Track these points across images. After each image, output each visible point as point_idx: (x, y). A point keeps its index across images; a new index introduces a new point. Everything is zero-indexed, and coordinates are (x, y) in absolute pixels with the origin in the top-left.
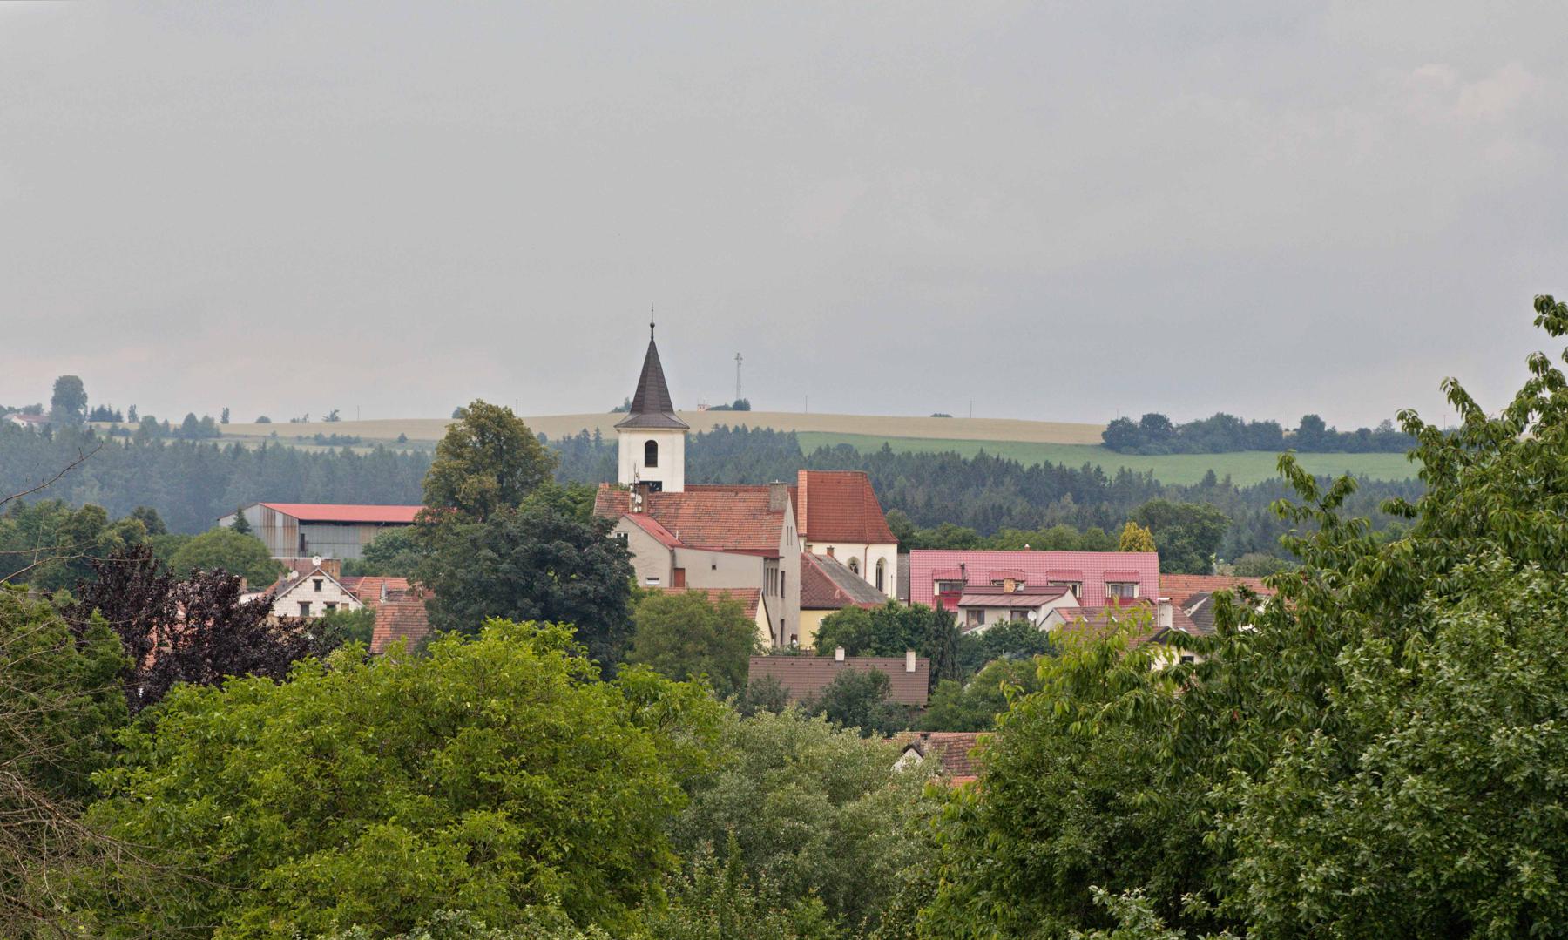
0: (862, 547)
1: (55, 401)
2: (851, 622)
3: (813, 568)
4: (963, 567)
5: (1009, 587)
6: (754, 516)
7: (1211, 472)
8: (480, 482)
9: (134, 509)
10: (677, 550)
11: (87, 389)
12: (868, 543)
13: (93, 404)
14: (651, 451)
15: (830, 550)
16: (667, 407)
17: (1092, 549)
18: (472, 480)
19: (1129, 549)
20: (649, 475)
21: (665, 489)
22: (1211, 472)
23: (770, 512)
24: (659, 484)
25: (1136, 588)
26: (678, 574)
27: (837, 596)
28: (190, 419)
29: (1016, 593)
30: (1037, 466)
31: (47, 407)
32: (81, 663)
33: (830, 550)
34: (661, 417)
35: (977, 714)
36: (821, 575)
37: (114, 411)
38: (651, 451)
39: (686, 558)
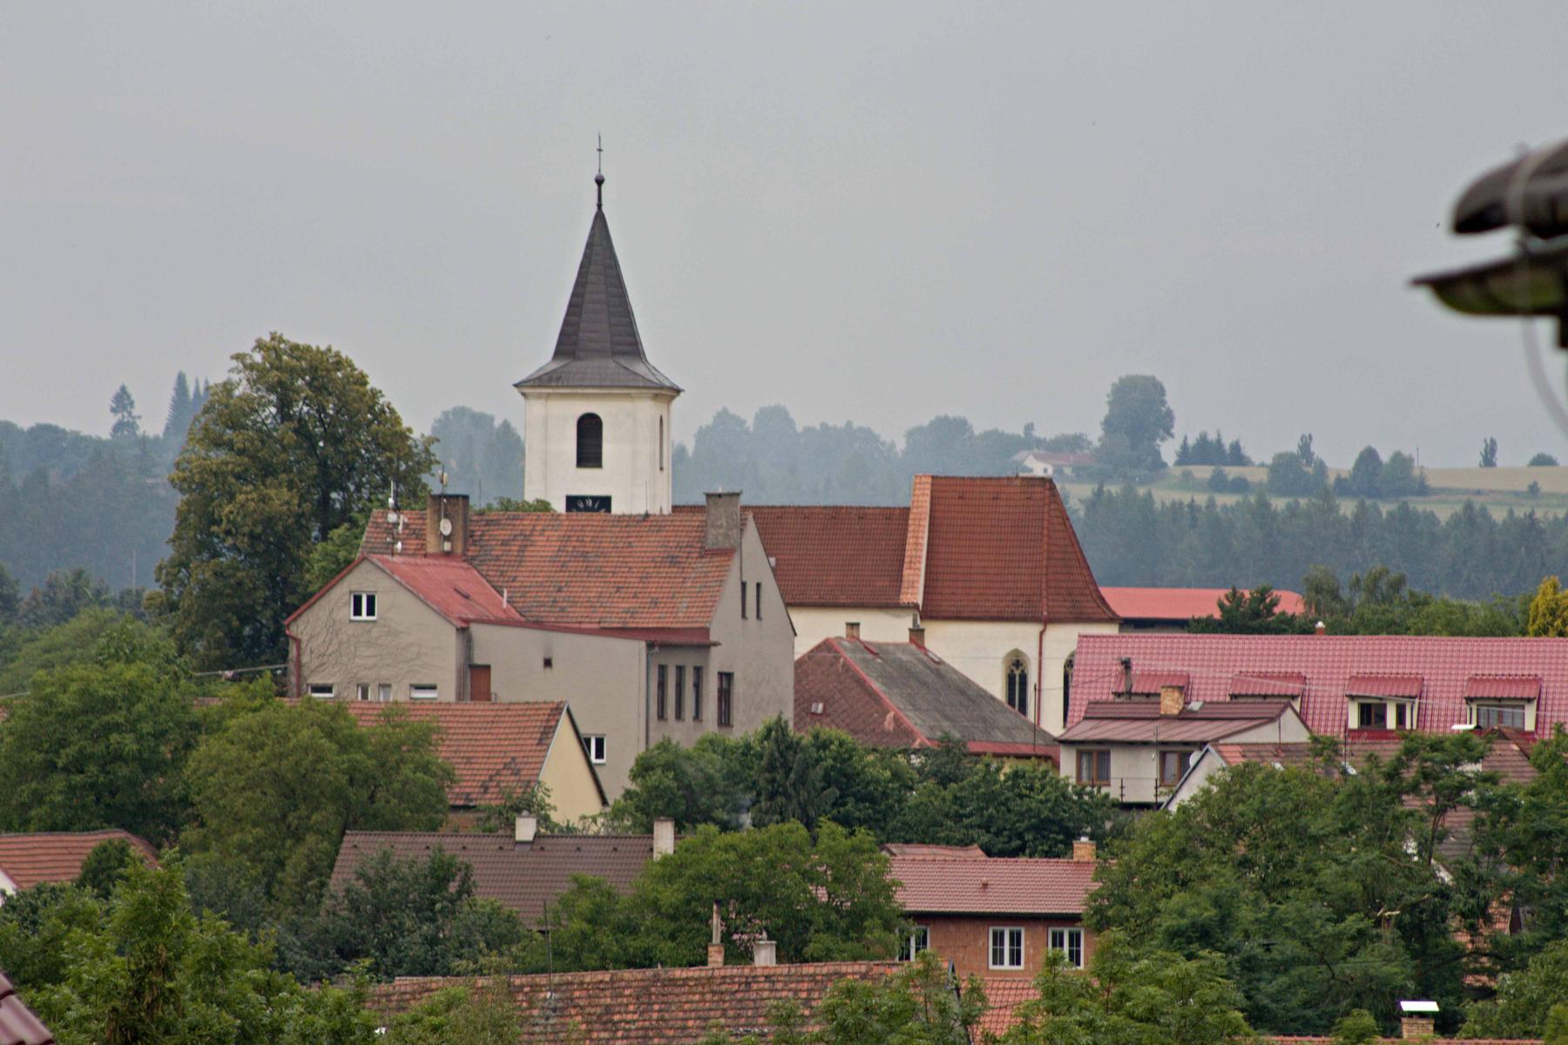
0: (1033, 629)
1: (1109, 424)
2: (667, 767)
3: (847, 667)
4: (1127, 664)
5: (1170, 703)
6: (673, 561)
7: (123, 389)
8: (264, 499)
9: (1124, 657)
10: (474, 628)
11: (1172, 400)
12: (1047, 621)
13: (1186, 429)
14: (589, 433)
15: (854, 626)
16: (633, 349)
17: (1493, 634)
18: (247, 495)
19: (1543, 631)
20: (589, 483)
21: (616, 509)
22: (123, 389)
23: (705, 553)
24: (604, 503)
25: (1530, 714)
26: (476, 677)
27: (888, 724)
28: (1369, 456)
29: (1185, 716)
30: (491, 419)
31: (1095, 434)
32: (627, 1013)
33: (917, 634)
34: (610, 365)
35: (633, 944)
36: (861, 683)
37: (1227, 443)
38: (589, 433)
39: (493, 644)
